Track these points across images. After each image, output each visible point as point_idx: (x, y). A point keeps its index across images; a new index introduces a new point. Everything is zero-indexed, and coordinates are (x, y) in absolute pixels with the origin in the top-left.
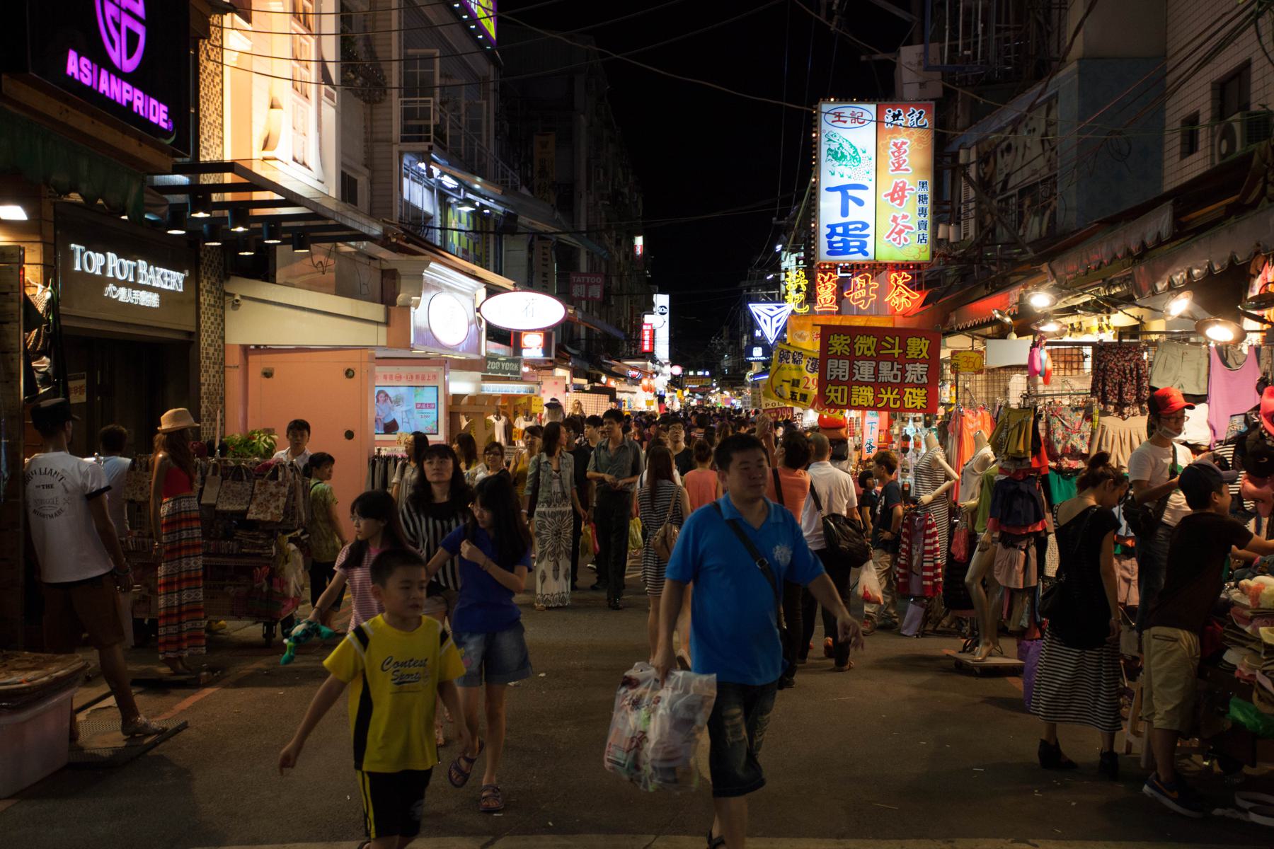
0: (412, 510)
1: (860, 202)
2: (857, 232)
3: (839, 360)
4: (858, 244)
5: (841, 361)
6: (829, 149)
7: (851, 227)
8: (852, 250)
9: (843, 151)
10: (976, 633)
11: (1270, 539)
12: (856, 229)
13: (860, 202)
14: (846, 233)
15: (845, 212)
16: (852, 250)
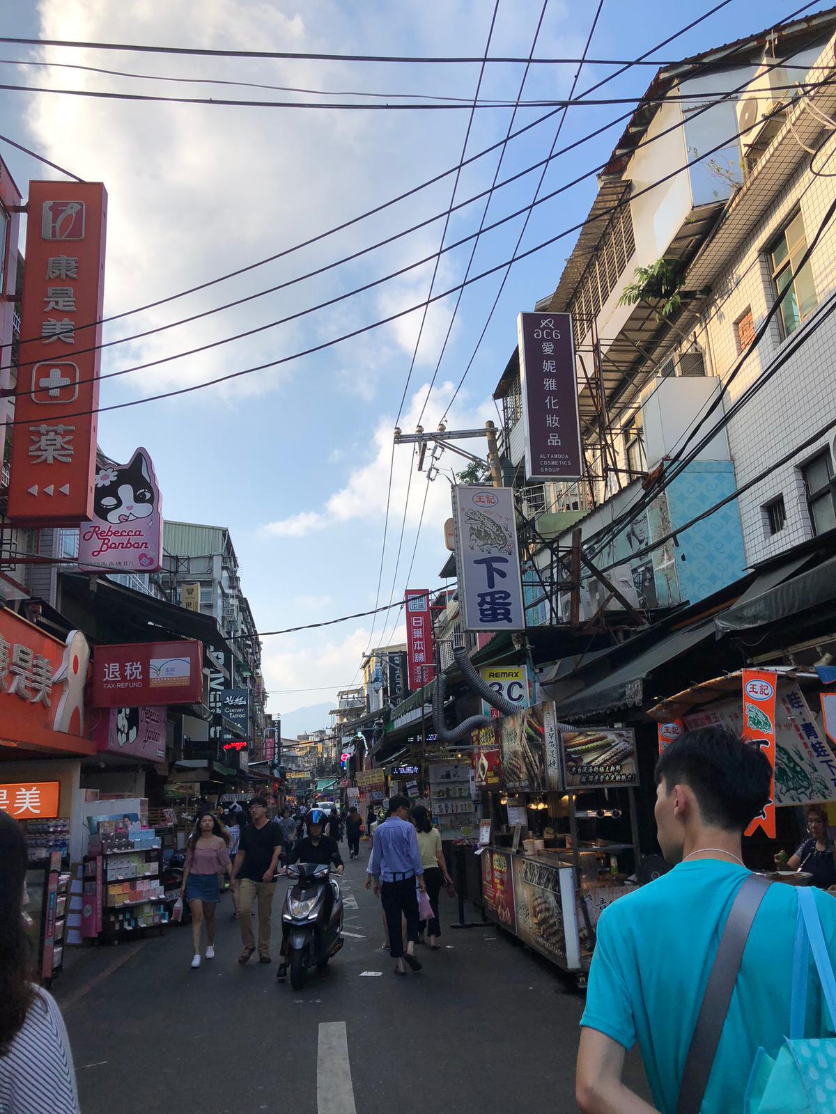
0: (359, 763)
1: (503, 575)
2: (501, 601)
3: (586, 566)
4: (503, 611)
5: (586, 568)
6: (471, 528)
7: (497, 596)
8: (499, 617)
9: (486, 529)
10: (798, 769)
11: (631, 838)
12: (500, 598)
13: (503, 575)
14: (493, 602)
15: (491, 585)
16: (499, 617)
